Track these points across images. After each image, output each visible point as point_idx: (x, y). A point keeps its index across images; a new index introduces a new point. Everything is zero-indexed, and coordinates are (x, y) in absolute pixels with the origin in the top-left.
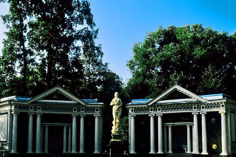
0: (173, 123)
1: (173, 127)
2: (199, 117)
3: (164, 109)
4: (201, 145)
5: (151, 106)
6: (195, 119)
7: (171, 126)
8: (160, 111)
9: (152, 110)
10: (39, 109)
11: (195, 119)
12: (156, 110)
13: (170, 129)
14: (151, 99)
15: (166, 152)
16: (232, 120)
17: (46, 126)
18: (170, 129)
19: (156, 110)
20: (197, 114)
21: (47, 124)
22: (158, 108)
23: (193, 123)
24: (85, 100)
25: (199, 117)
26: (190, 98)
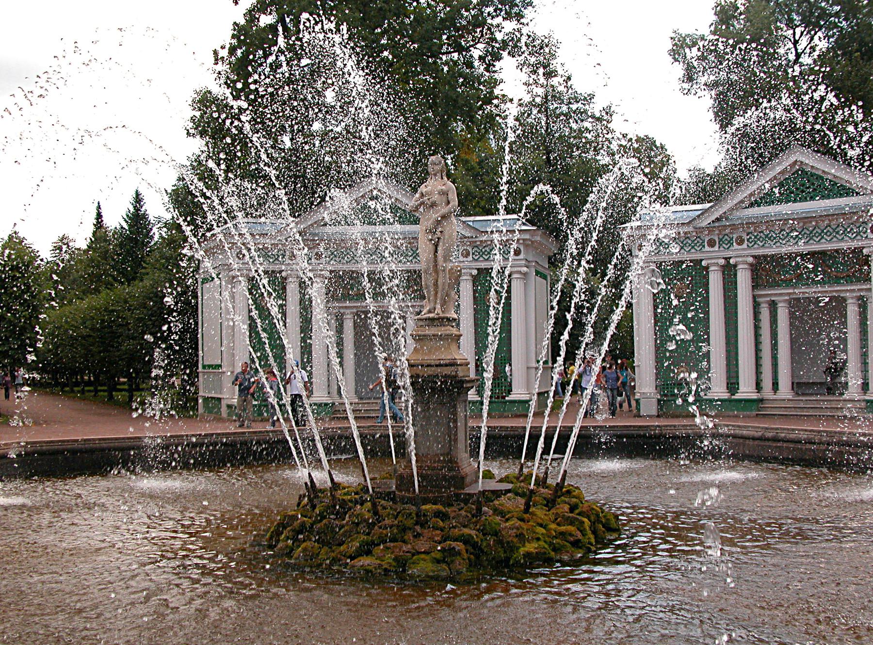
0: (791, 291)
1: (795, 304)
2: (729, 271)
3: (759, 240)
4: (733, 354)
5: (710, 229)
6: (715, 280)
7: (785, 301)
8: (716, 248)
9: (711, 243)
10: (740, 242)
11: (715, 280)
12: (729, 242)
13: (783, 314)
14: (708, 205)
15: (767, 391)
16: (538, 297)
17: (844, 300)
18: (783, 314)
19: (729, 242)
20: (722, 262)
21: (781, 294)
22: (735, 236)
23: (868, 286)
24: (472, 218)
25: (729, 271)
26: (846, 191)
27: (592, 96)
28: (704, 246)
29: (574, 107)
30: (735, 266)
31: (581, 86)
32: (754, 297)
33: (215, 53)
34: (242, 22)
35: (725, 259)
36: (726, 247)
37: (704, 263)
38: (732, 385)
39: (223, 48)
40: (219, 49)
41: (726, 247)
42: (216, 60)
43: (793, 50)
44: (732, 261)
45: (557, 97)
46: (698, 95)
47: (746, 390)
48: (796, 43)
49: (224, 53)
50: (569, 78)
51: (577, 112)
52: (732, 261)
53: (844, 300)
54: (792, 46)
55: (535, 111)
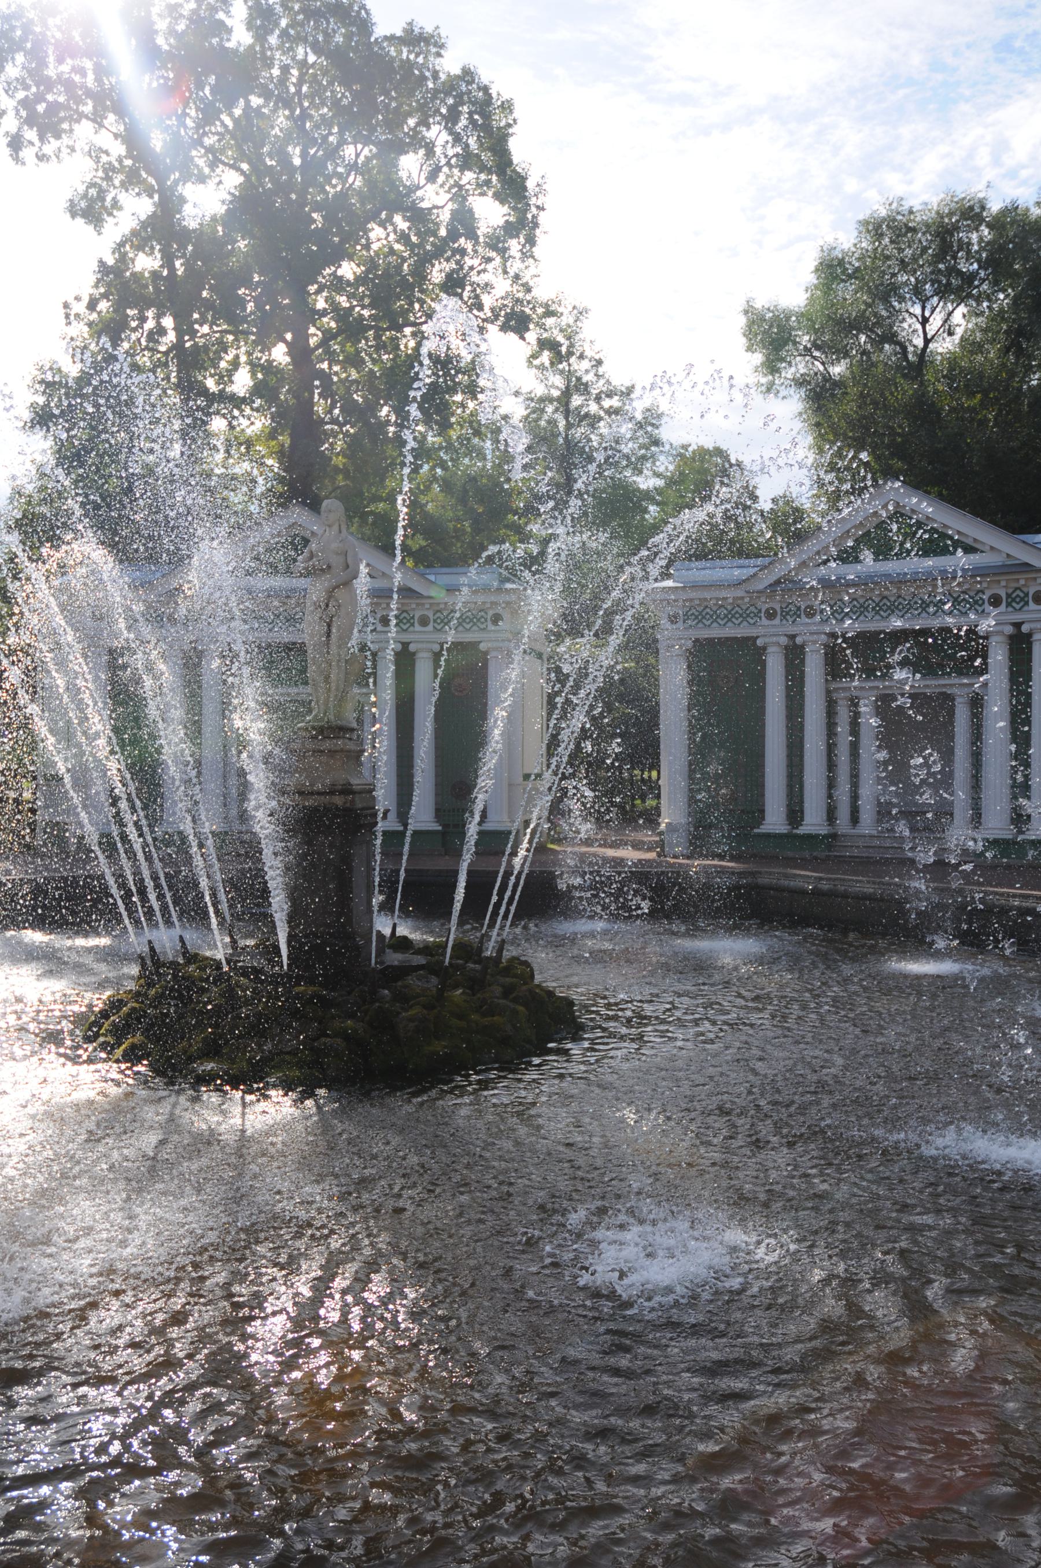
2: (794, 654)
8: (777, 621)
12: (1022, 599)
17: (950, 698)
20: (784, 641)
25: (794, 654)
27: (630, 390)
28: (413, 625)
29: (607, 403)
30: (764, 648)
31: (617, 374)
32: (828, 692)
33: (66, 306)
34: (110, 261)
35: (403, 644)
36: (1018, 607)
37: (1025, 628)
38: (795, 814)
39: (78, 299)
40: (71, 300)
41: (1018, 607)
42: (67, 316)
43: (920, 332)
44: (1025, 628)
45: (583, 388)
46: (781, 395)
47: (813, 822)
48: (925, 321)
49: (80, 308)
50: (599, 362)
51: (611, 412)
52: (412, 648)
53: (950, 698)
54: (919, 327)
55: (550, 409)
